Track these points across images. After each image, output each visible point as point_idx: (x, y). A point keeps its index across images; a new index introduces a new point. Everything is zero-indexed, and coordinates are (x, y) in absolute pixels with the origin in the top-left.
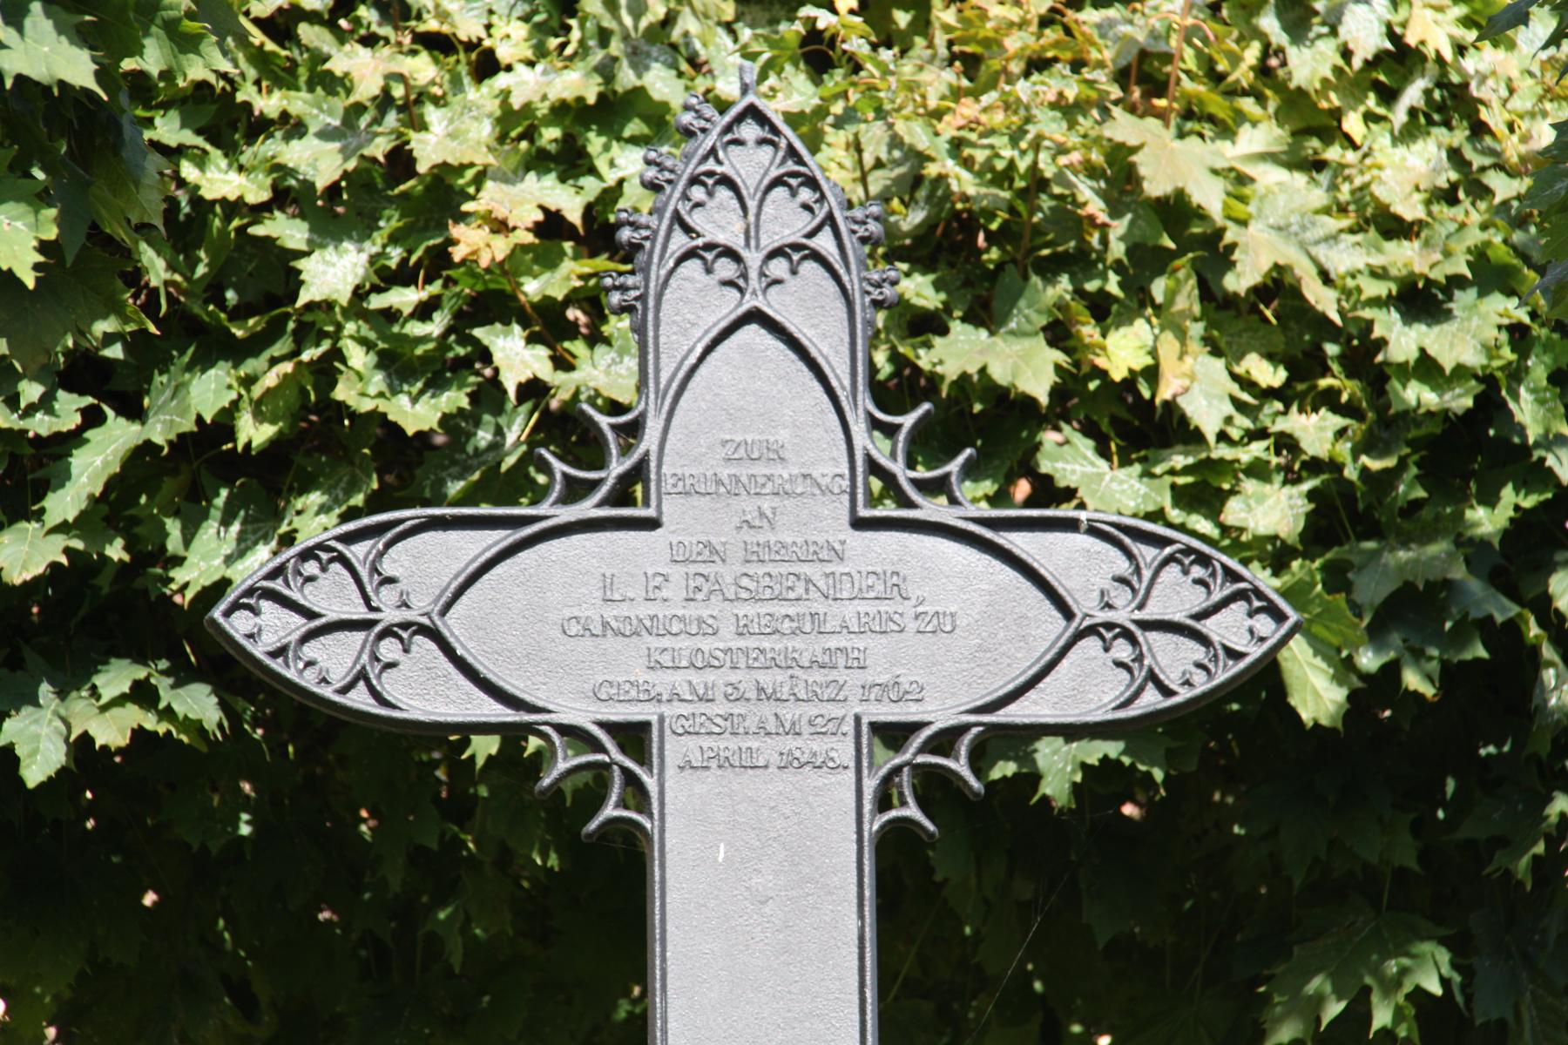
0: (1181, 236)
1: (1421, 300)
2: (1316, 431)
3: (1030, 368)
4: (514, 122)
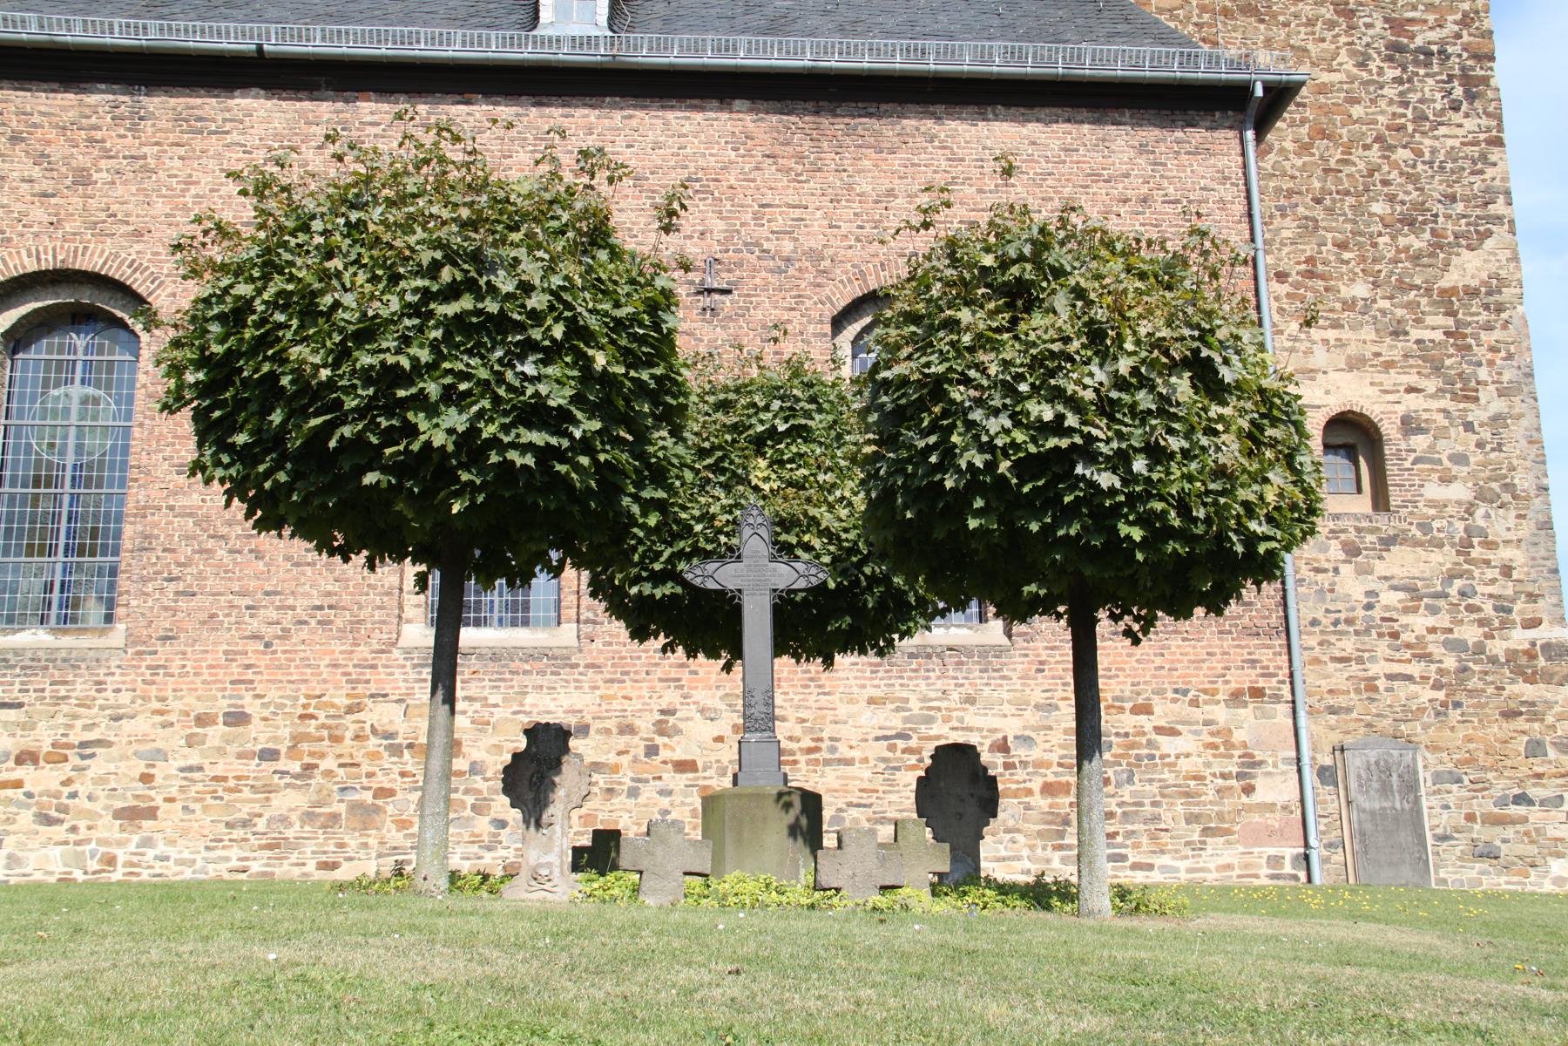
0: (814, 521)
1: (846, 530)
2: (832, 548)
3: (794, 540)
4: (723, 507)
